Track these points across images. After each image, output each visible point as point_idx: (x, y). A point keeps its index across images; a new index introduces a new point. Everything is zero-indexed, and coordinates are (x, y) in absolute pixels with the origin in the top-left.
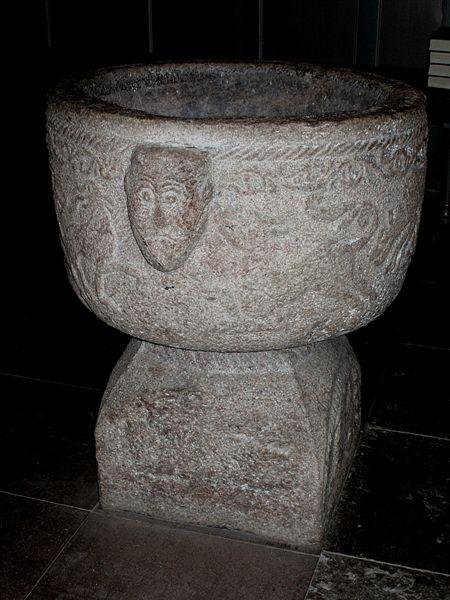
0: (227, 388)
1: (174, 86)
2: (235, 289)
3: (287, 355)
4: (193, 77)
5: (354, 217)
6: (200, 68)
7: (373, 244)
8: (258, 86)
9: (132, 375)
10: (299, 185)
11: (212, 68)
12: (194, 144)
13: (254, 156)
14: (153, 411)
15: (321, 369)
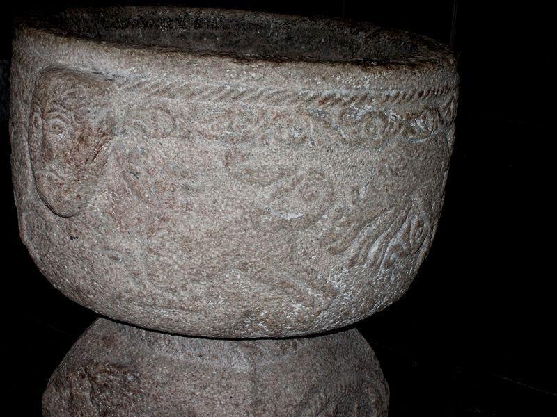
0: (168, 375)
1: (214, 31)
2: (141, 251)
3: (248, 350)
4: (239, 25)
5: (293, 185)
6: (248, 17)
7: (325, 224)
8: (309, 43)
9: (90, 343)
10: (218, 134)
11: (262, 18)
12: (101, 69)
13: (164, 91)
14: (95, 386)
15: (295, 377)
